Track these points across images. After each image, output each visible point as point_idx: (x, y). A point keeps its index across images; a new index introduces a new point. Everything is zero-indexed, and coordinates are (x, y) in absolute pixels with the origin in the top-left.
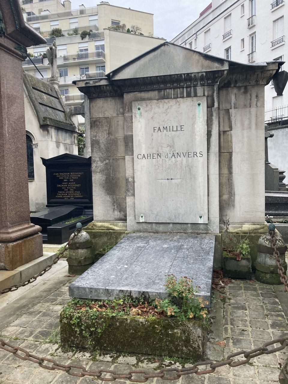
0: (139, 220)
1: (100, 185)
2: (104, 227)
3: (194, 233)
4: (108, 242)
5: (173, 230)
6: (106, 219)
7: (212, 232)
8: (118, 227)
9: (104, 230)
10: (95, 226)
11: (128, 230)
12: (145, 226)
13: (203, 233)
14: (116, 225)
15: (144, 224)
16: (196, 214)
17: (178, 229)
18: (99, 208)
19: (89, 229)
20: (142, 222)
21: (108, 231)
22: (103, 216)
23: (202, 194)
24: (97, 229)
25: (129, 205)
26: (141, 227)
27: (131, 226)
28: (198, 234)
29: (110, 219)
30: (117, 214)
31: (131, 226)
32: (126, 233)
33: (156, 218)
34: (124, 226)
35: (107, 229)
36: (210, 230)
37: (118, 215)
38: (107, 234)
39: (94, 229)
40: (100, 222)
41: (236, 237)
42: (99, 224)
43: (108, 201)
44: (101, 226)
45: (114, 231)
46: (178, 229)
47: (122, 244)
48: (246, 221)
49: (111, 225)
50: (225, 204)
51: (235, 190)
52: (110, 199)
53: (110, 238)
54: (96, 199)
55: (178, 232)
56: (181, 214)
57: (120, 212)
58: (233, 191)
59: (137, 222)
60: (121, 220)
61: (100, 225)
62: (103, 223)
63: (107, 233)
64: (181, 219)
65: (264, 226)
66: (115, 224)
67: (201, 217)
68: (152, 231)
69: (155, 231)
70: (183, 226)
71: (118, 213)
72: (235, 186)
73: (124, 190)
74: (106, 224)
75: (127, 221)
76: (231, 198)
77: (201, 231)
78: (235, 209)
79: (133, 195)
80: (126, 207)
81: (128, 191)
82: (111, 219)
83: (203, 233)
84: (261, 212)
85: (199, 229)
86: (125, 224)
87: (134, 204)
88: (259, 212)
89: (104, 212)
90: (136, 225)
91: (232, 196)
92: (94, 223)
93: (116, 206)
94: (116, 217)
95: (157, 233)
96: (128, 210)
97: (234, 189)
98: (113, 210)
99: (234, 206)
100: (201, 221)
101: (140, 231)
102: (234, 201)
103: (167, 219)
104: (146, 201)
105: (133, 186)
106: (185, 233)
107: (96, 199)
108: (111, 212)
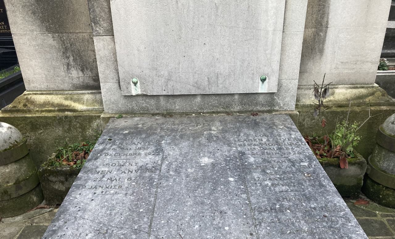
0: (130, 92)
1: (23, 7)
2: (53, 105)
3: (246, 112)
4: (65, 137)
5: (201, 109)
6: (52, 86)
7: (280, 107)
8: (83, 104)
9: (54, 111)
10: (32, 102)
11: (106, 111)
12: (143, 103)
13: (263, 112)
14: (78, 101)
15: (140, 100)
16: (253, 74)
17: (213, 107)
18: (33, 63)
19: (18, 111)
20: (138, 95)
21: (61, 114)
22: (47, 79)
23: (271, 29)
24: (37, 111)
25: (101, 57)
26: (133, 105)
27: (113, 103)
28: (255, 114)
29: (62, 87)
30: (76, 75)
31: (113, 103)
32: (103, 118)
33: (167, 85)
34: (95, 101)
35: (59, 111)
36: (278, 104)
37: (79, 78)
38: (60, 121)
39: (30, 111)
40: (42, 94)
41: (324, 116)
42: (41, 99)
43: (51, 46)
44: (45, 104)
45: (75, 114)
46: (213, 107)
47: (99, 162)
48: (340, 81)
49: (66, 99)
50: (312, 47)
51: (330, 17)
52: (54, 43)
53: (69, 129)
54: (21, 41)
55: (214, 112)
56: (221, 74)
57: (82, 70)
58: (325, 20)
59: (126, 96)
60: (86, 87)
61: (42, 101)
62: (48, 96)
63: (61, 118)
64: (221, 86)
65: (375, 89)
66: (75, 97)
67: (263, 80)
68: (158, 112)
69: (165, 112)
70: (222, 99)
71: (78, 74)
72: (331, 7)
73: (84, 20)
74: (56, 99)
75: (102, 91)
76: (318, 35)
77: (259, 108)
78: (324, 57)
79: (110, 32)
80: (95, 60)
81: (94, 23)
82: (66, 86)
83: (263, 112)
84: (372, 63)
85: (257, 104)
86: (98, 96)
87: (115, 54)
88: (367, 62)
89: (46, 73)
90: (123, 101)
91: (321, 31)
92: (29, 97)
93: (71, 58)
94: (75, 81)
95: (171, 116)
96: (101, 69)
97: (328, 14)
98: (66, 67)
99: (321, 51)
100: (263, 88)
101: (132, 113)
102: (323, 42)
103: (192, 87)
104: (142, 48)
105: (107, 10)
106: (228, 113)
107: (21, 41)
108: (62, 71)
